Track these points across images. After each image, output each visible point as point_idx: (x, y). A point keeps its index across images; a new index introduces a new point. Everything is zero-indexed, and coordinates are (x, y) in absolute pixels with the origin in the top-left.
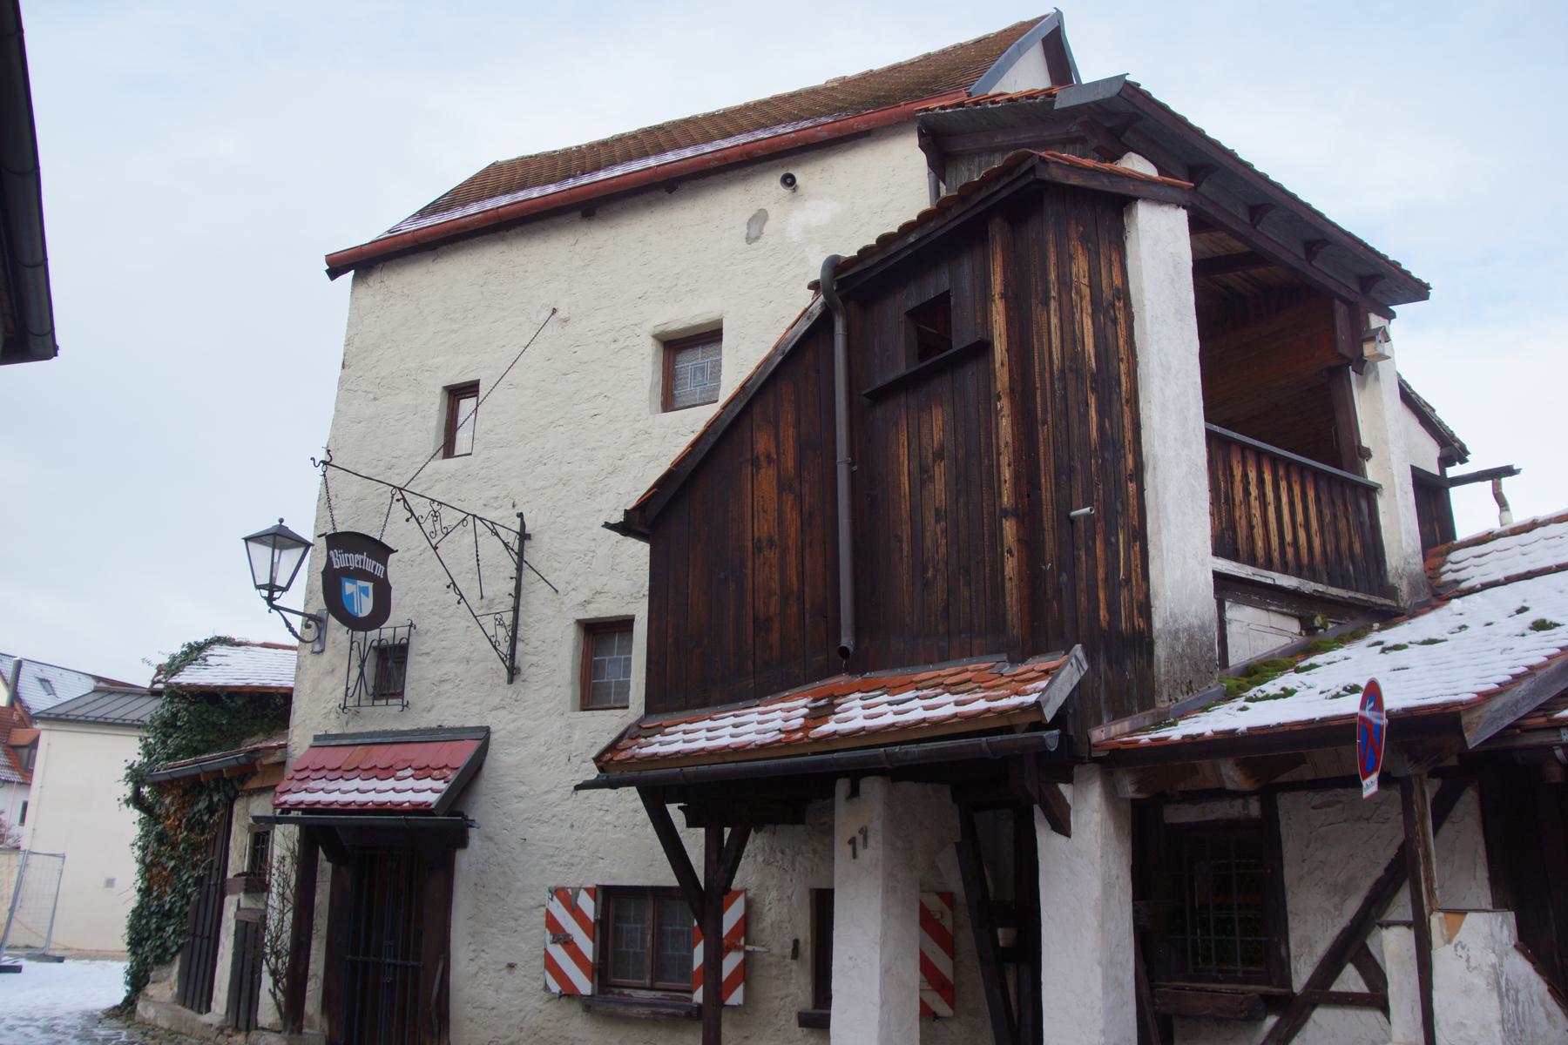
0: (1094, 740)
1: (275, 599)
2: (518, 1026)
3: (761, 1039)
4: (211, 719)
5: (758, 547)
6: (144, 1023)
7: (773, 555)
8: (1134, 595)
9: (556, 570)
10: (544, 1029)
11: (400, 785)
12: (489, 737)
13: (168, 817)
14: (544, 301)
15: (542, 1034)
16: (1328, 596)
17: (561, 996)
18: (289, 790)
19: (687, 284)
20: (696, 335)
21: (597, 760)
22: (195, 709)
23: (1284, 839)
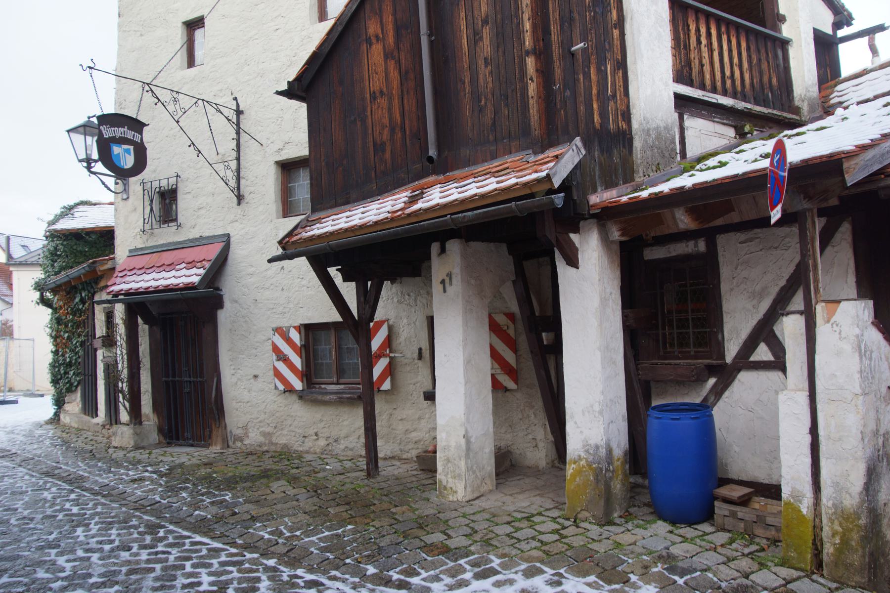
0: (591, 203)
1: (92, 167)
3: (403, 409)
4: (78, 249)
5: (373, 97)
6: (65, 426)
7: (384, 102)
8: (618, 106)
10: (278, 411)
12: (230, 240)
15: (277, 415)
16: (754, 112)
17: (285, 392)
18: (115, 283)
21: (280, 242)
23: (721, 265)
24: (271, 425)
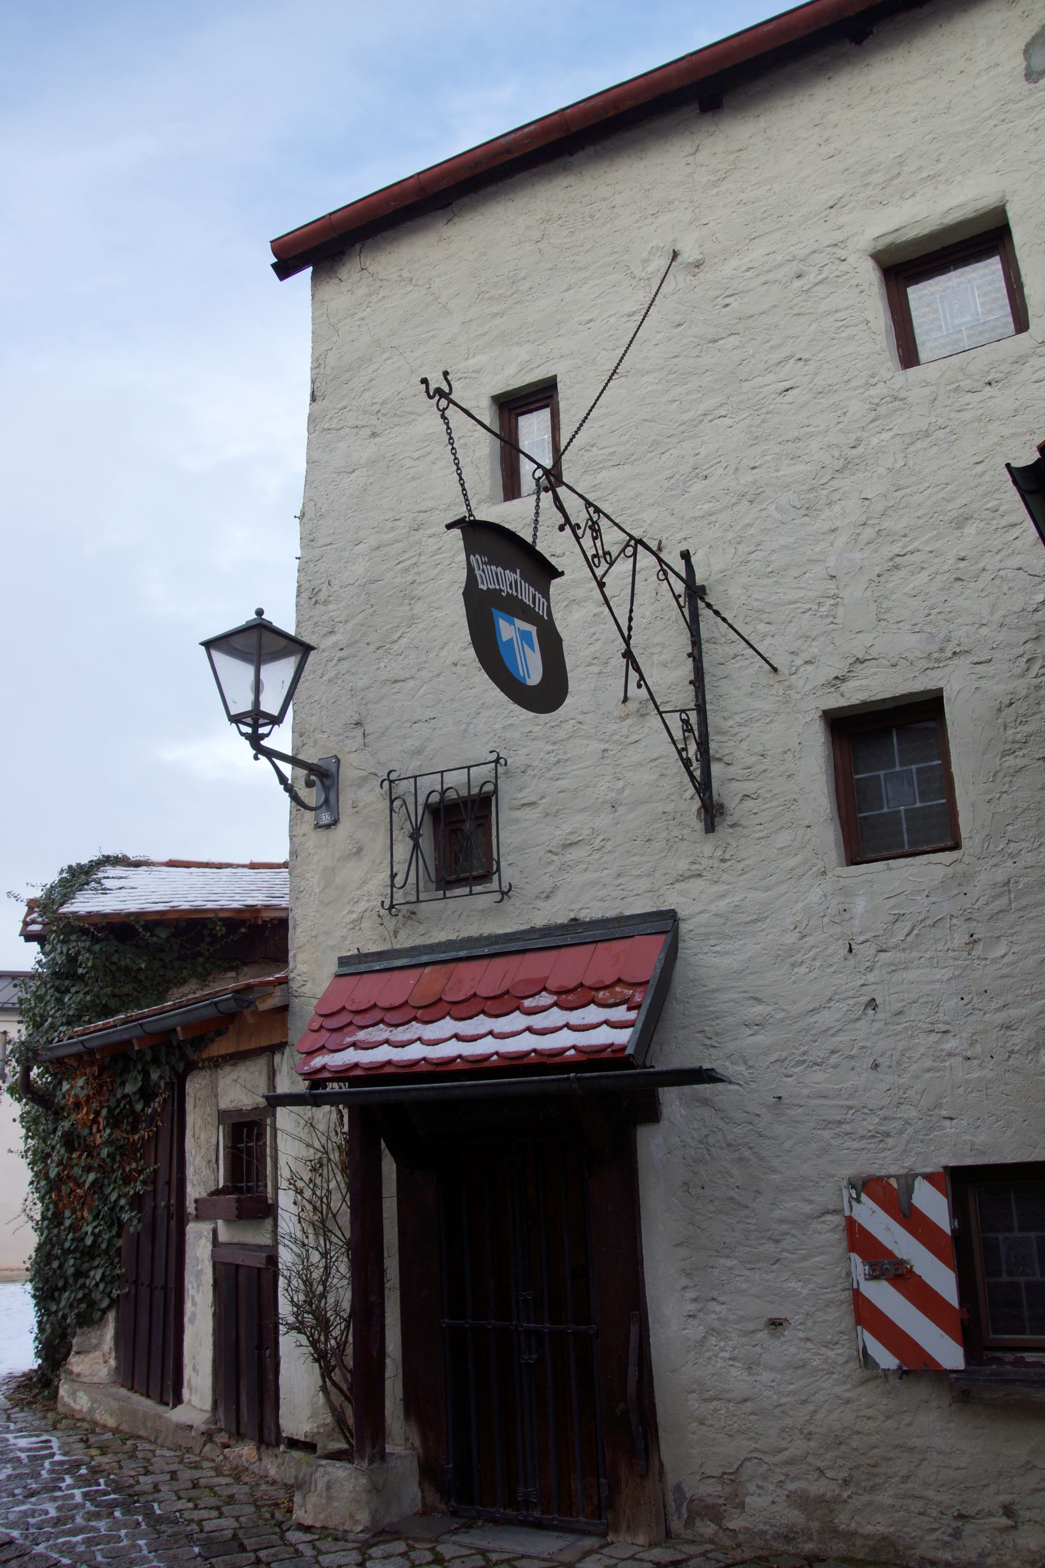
2: (801, 1431)
9: (765, 636)
11: (539, 1021)
13: (77, 1106)
14: (654, 243)
19: (920, 169)
20: (943, 249)
22: (101, 949)
24: (830, 1474)
